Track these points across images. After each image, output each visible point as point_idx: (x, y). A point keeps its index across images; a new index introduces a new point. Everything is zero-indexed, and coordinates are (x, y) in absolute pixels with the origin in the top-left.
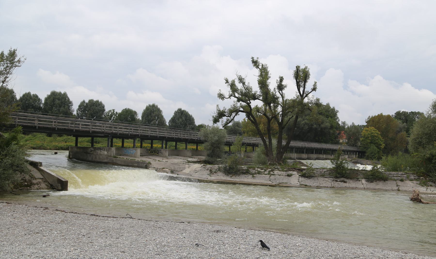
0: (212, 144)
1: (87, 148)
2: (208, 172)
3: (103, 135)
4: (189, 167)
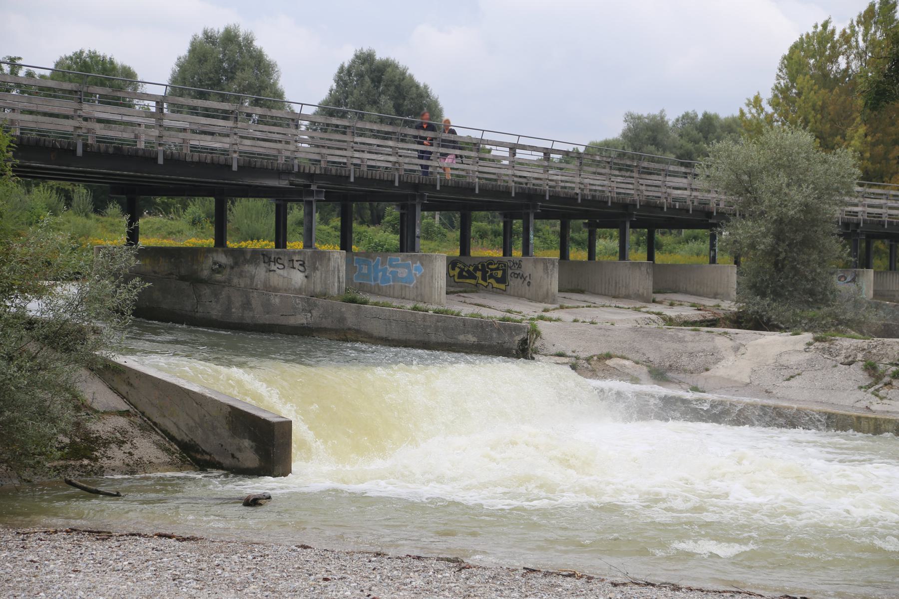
0: (783, 229)
1: (194, 252)
2: (858, 373)
3: (283, 183)
4: (736, 349)
